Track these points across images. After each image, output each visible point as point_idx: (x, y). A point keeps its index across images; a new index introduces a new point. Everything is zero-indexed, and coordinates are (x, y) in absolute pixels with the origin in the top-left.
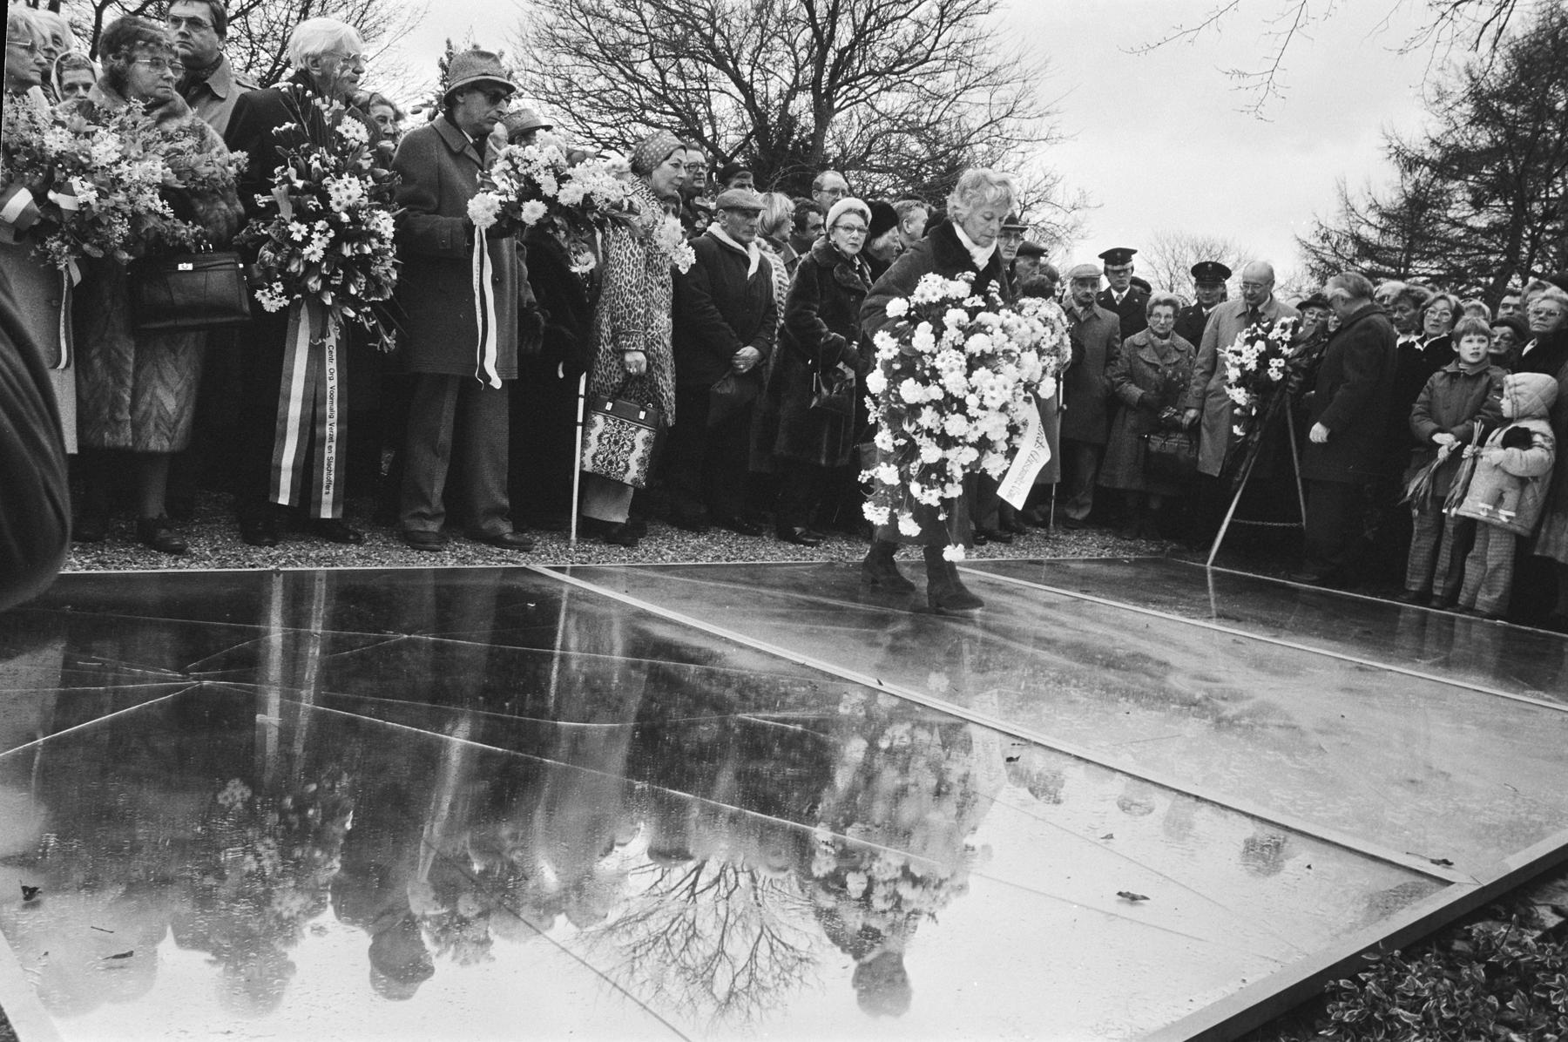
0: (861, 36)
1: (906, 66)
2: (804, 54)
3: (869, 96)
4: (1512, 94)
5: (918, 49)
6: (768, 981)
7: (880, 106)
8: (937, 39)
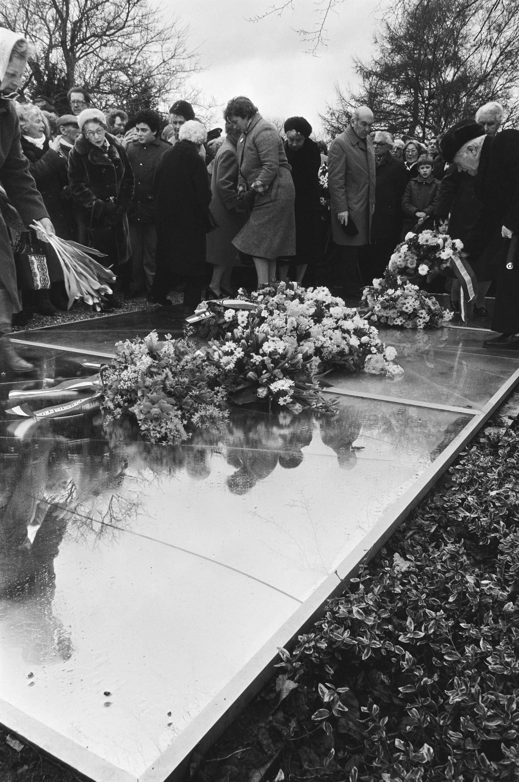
0: (85, 14)
1: (113, 31)
2: (52, 25)
3: (95, 50)
4: (409, 37)
5: (117, 21)
6: (120, 517)
7: (104, 56)
8: (128, 14)
